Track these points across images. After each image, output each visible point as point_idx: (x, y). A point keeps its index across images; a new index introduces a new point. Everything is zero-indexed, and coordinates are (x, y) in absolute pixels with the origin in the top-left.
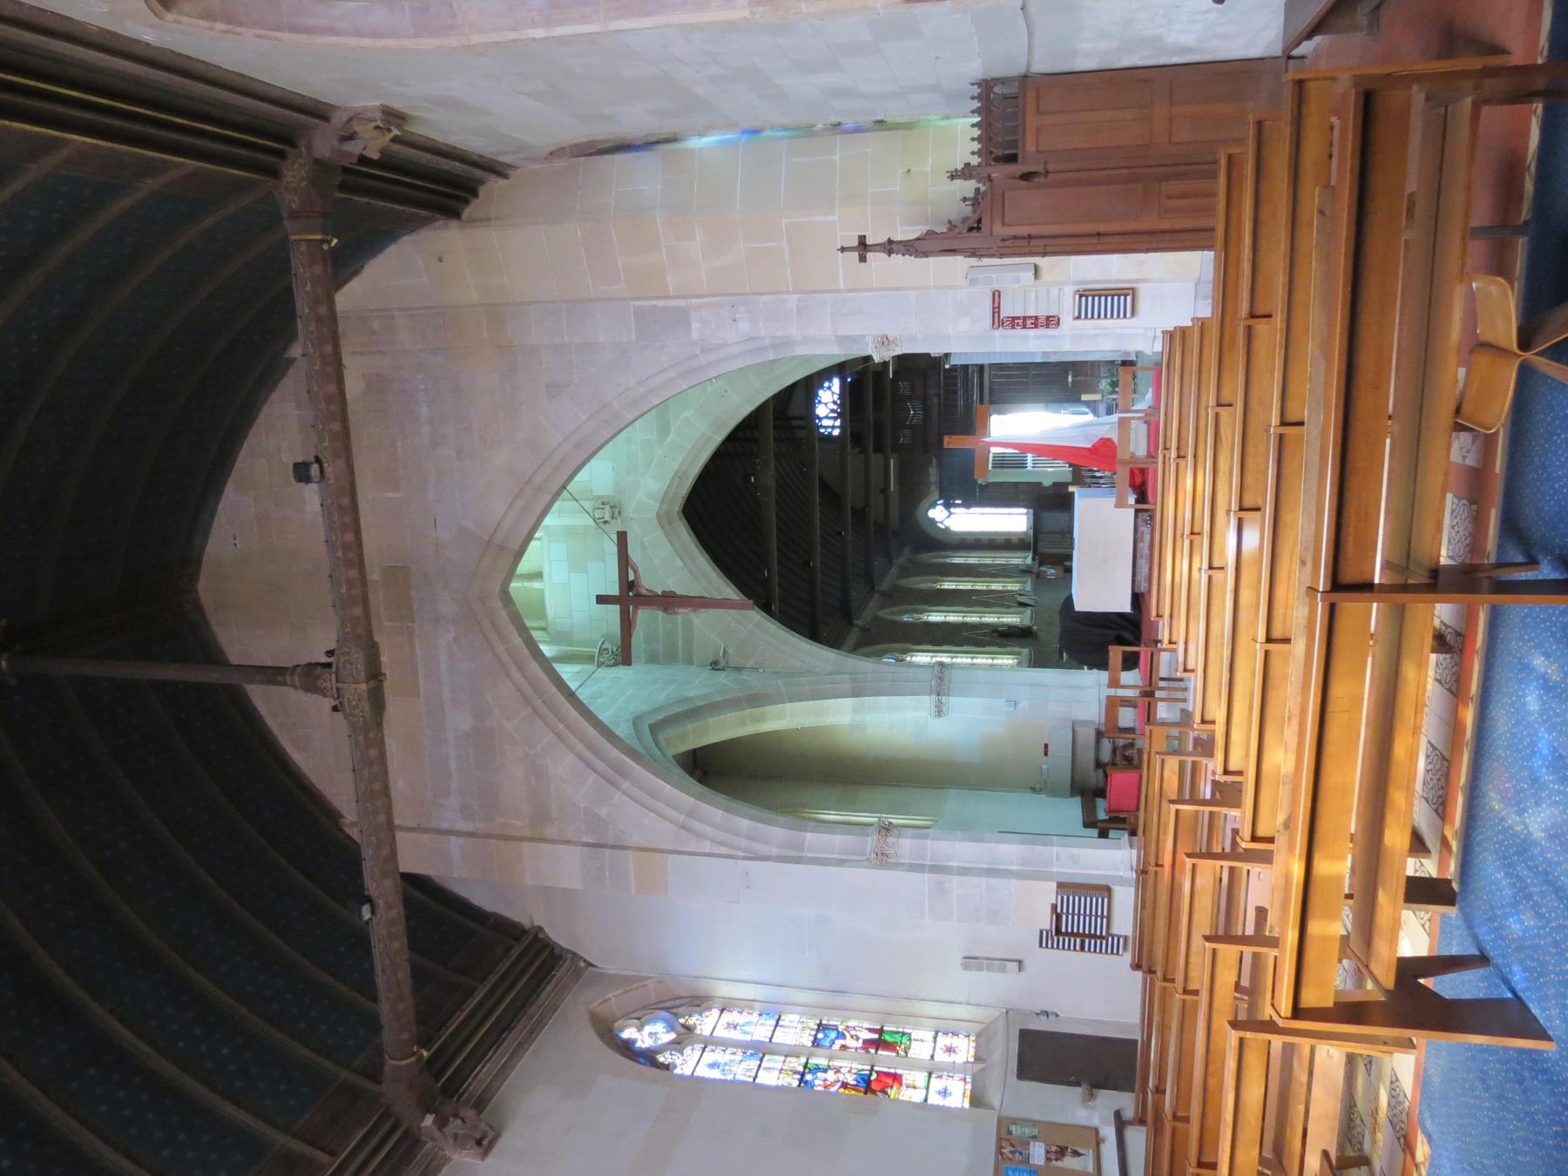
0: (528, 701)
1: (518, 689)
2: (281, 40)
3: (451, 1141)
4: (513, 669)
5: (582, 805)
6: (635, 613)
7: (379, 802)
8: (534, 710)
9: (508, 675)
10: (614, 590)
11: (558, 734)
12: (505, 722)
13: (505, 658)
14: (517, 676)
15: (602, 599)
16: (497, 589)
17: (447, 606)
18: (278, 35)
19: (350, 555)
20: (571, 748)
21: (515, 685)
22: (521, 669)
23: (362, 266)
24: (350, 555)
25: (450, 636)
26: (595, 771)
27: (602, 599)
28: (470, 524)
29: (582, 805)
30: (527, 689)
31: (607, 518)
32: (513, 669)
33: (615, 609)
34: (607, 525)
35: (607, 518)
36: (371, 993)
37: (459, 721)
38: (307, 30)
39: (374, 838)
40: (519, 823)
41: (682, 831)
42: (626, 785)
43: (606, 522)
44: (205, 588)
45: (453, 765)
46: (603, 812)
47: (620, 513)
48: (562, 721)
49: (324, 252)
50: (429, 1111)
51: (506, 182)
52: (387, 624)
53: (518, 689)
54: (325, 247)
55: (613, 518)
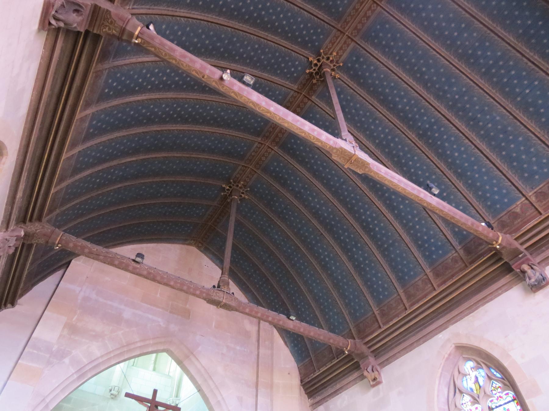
0: (128, 345)
1: (134, 343)
2: (439, 369)
3: (8, 238)
4: (142, 344)
5: (73, 351)
6: (146, 406)
7: (179, 285)
8: (123, 346)
9: (141, 341)
10: (158, 399)
11: (110, 352)
12: (122, 331)
13: (147, 342)
14: (139, 344)
15: (155, 392)
16: (171, 349)
17: (173, 327)
18: (440, 369)
19: (265, 317)
20: (102, 356)
21: (136, 342)
22: (140, 347)
23: (288, 347)
24: (265, 317)
25: (162, 324)
26: (88, 364)
27: (155, 392)
28: (200, 349)
29: (73, 351)
30: (132, 347)
31: (112, 392)
32: (142, 344)
33: (150, 397)
34: (109, 391)
35: (112, 392)
36: (87, 239)
37: (128, 313)
38: (440, 377)
39: (166, 277)
40: (74, 319)
41: (42, 399)
42: (75, 376)
43: (111, 390)
44: (194, 249)
45: (109, 303)
46: (67, 360)
47: (112, 398)
48: (114, 356)
49: (343, 348)
50: (25, 235)
51: (308, 406)
52: (188, 306)
53: (134, 343)
54: (345, 349)
55: (112, 394)
